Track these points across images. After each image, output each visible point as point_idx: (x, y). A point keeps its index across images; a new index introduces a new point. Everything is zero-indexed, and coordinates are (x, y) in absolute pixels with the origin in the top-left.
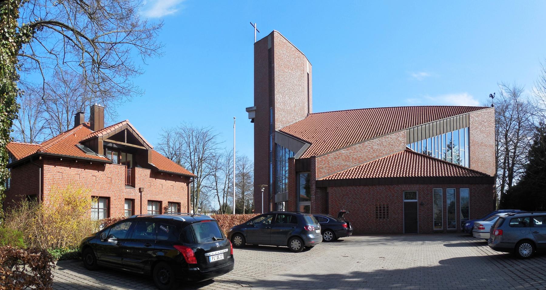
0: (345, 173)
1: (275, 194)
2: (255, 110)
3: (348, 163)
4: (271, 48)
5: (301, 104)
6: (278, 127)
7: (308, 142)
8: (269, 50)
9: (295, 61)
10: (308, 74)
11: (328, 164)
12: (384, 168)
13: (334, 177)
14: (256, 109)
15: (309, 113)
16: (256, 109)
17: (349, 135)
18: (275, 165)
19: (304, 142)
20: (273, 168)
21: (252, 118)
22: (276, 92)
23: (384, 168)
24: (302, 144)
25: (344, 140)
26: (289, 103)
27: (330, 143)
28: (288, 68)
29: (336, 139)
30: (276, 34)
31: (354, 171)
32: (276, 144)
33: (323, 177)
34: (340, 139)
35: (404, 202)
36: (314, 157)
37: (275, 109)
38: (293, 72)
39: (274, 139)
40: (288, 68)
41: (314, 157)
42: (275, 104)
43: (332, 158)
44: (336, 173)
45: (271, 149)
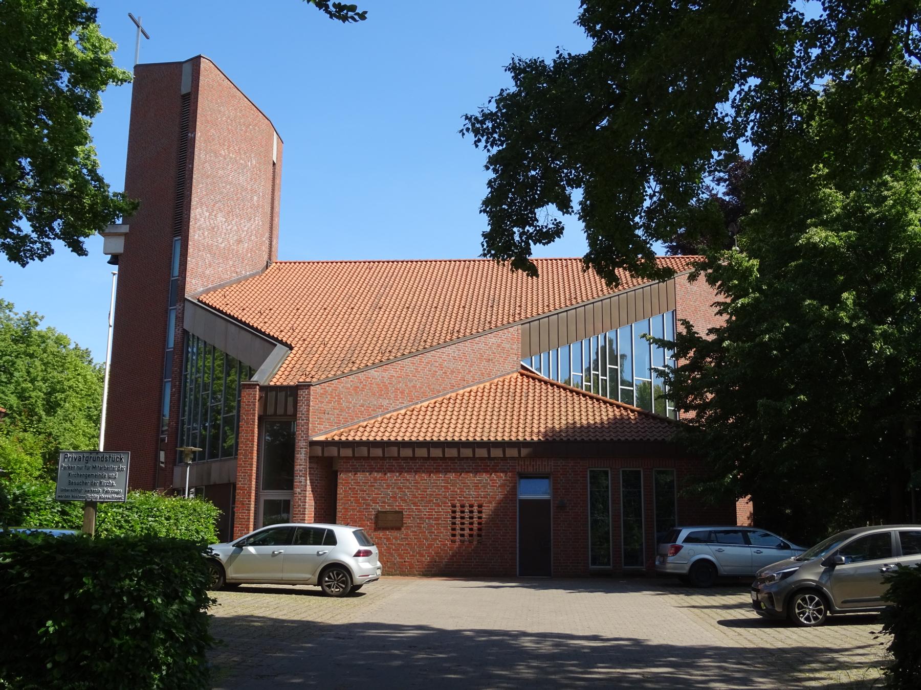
0: (377, 425)
1: (175, 465)
2: (126, 234)
3: (385, 403)
4: (189, 94)
5: (253, 238)
6: (194, 287)
7: (286, 344)
8: (183, 96)
9: (246, 132)
10: (274, 164)
11: (339, 403)
12: (420, 292)
13: (352, 433)
14: (127, 231)
15: (270, 259)
16: (127, 231)
17: (438, 425)
18: (180, 386)
19: (271, 342)
20: (172, 395)
21: (113, 252)
22: (194, 202)
23: (420, 292)
24: (267, 344)
25: (319, 285)
26: (224, 231)
27: (307, 325)
28: (229, 146)
29: (314, 304)
30: (204, 64)
31: (399, 421)
32: (185, 332)
33: (326, 433)
34: (328, 301)
35: (521, 501)
36: (308, 386)
37: (190, 243)
38: (241, 158)
39: (180, 319)
40: (229, 146)
41: (308, 386)
42: (191, 231)
43: (349, 389)
44: (356, 423)
45: (171, 344)
